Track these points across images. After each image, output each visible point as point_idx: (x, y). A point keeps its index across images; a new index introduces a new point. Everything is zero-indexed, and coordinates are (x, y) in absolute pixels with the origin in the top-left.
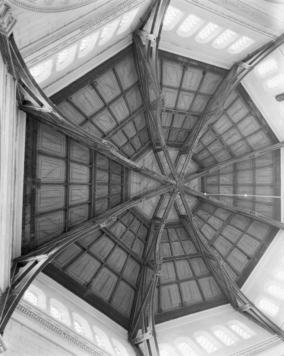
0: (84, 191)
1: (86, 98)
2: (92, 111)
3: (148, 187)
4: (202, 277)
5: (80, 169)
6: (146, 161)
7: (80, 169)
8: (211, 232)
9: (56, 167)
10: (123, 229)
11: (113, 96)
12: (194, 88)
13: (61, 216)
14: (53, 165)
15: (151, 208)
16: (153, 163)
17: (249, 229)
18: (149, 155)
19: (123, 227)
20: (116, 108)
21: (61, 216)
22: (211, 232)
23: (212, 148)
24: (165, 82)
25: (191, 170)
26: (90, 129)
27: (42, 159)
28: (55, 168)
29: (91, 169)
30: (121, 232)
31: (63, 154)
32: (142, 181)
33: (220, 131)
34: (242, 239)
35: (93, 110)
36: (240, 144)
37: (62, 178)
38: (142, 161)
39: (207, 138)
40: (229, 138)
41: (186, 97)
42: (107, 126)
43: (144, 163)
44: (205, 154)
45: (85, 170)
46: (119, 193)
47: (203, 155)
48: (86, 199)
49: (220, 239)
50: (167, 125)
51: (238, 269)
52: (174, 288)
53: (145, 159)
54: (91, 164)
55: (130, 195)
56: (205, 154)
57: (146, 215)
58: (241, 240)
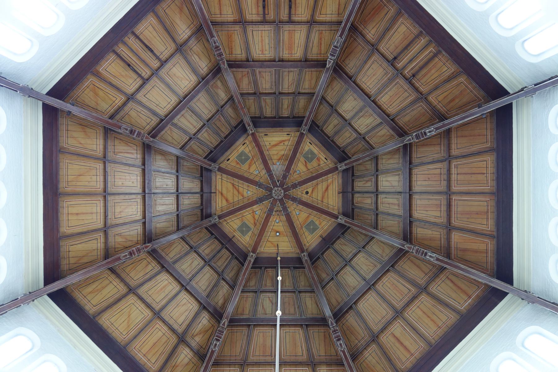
0: (185, 301)
1: (77, 214)
2: (99, 217)
3: (257, 219)
4: (412, 301)
5: (157, 283)
6: (224, 192)
7: (157, 283)
8: (395, 201)
9: (129, 310)
10: (271, 298)
11: (98, 177)
12: (169, 48)
13: (184, 352)
14: (124, 310)
15: (286, 239)
16: (233, 185)
17: (453, 146)
18: (220, 180)
19: (270, 296)
20: (119, 182)
21: (184, 352)
22: (395, 201)
23: (286, 86)
24: (130, 88)
25: (290, 142)
26: (119, 235)
27: (108, 317)
28: (129, 312)
29: (168, 271)
30: (273, 304)
31: (123, 289)
32: (242, 219)
33: (268, 54)
34: (453, 171)
35: (98, 214)
36: (315, 37)
37: (148, 313)
38: (220, 196)
39: (264, 82)
40: (290, 48)
41: (174, 70)
42: (134, 210)
43: (224, 197)
44: (286, 102)
45: (164, 279)
46: (231, 259)
47: (285, 106)
48: (193, 306)
49: (419, 202)
50: (98, 208)
51: (484, 227)
52: (397, 328)
53: (220, 190)
54: (163, 267)
55: (246, 247)
56: (286, 102)
57: (288, 253)
58: (454, 177)
